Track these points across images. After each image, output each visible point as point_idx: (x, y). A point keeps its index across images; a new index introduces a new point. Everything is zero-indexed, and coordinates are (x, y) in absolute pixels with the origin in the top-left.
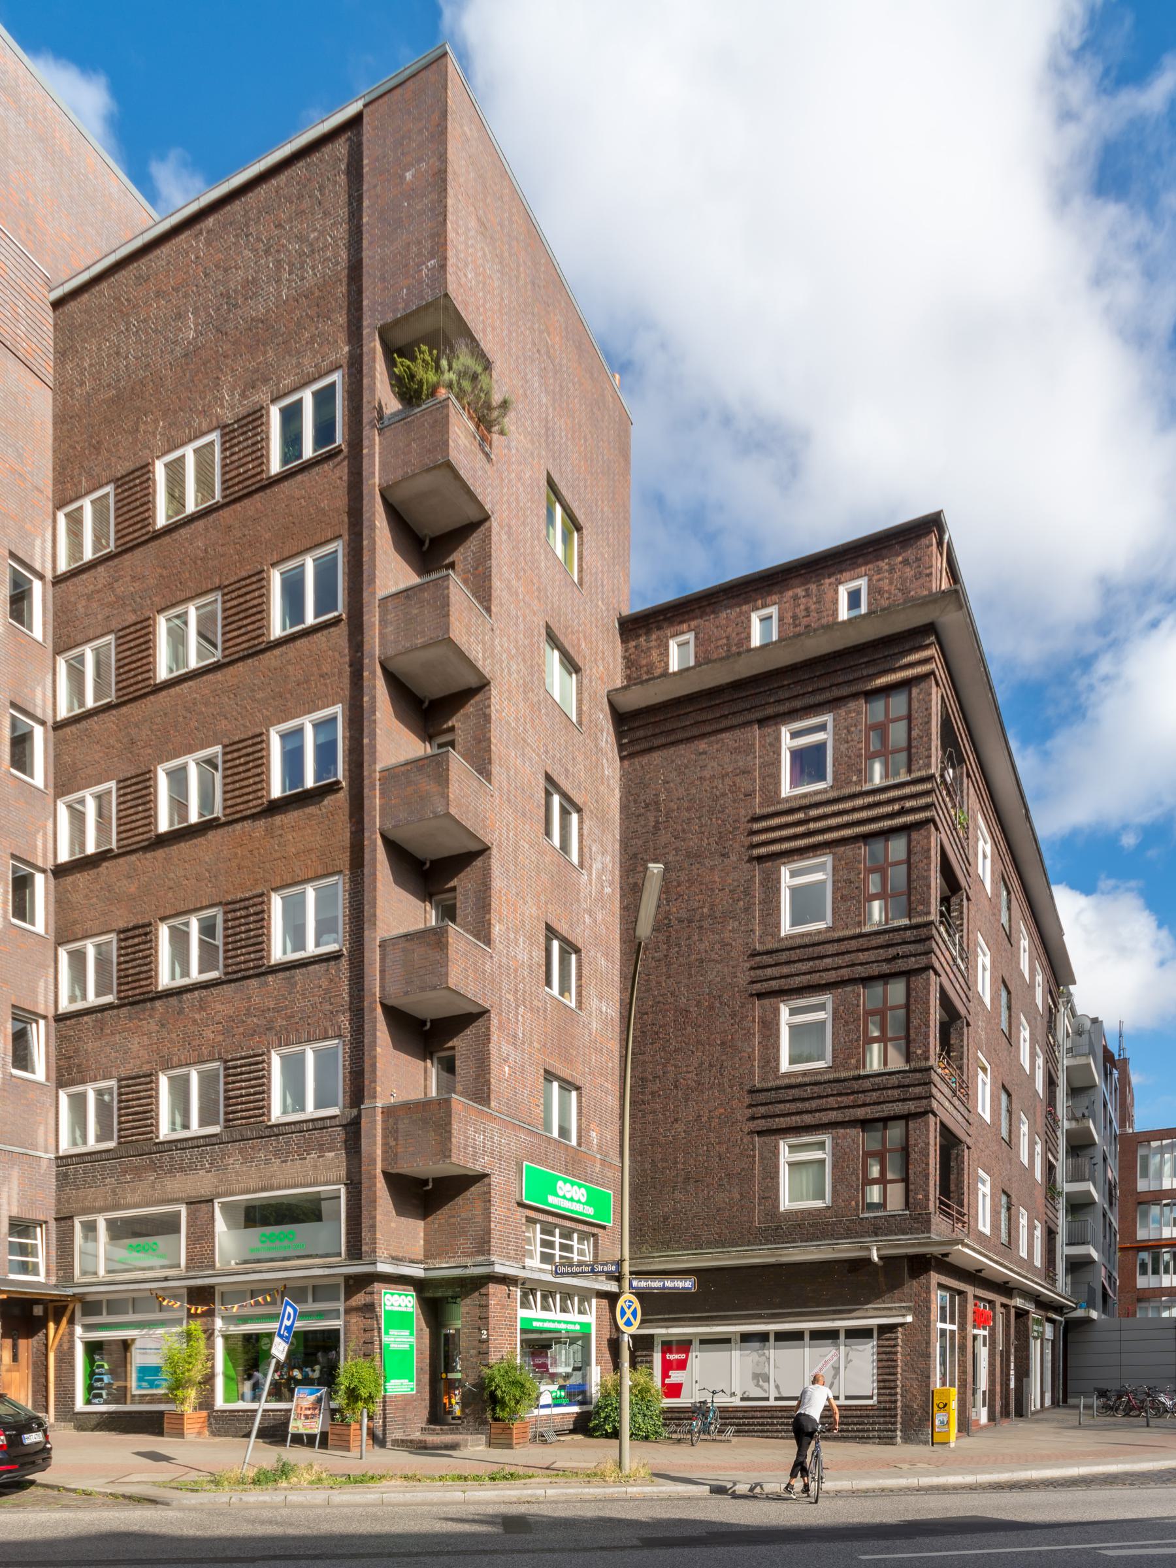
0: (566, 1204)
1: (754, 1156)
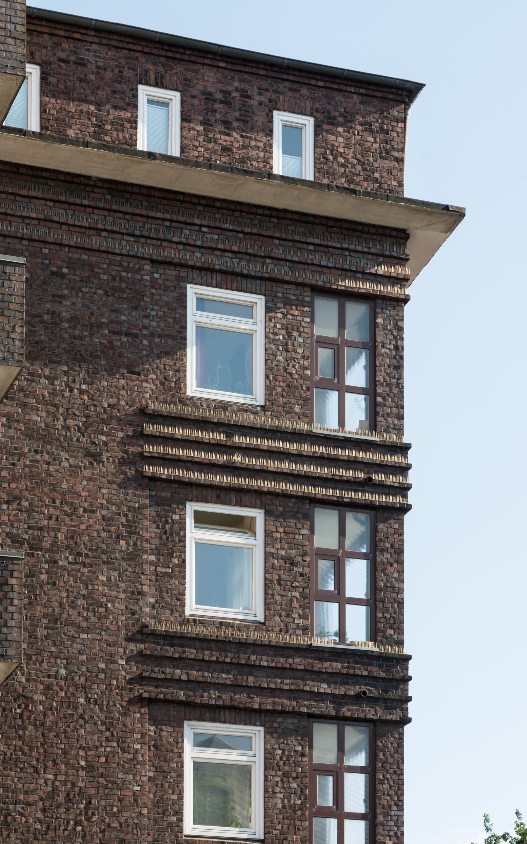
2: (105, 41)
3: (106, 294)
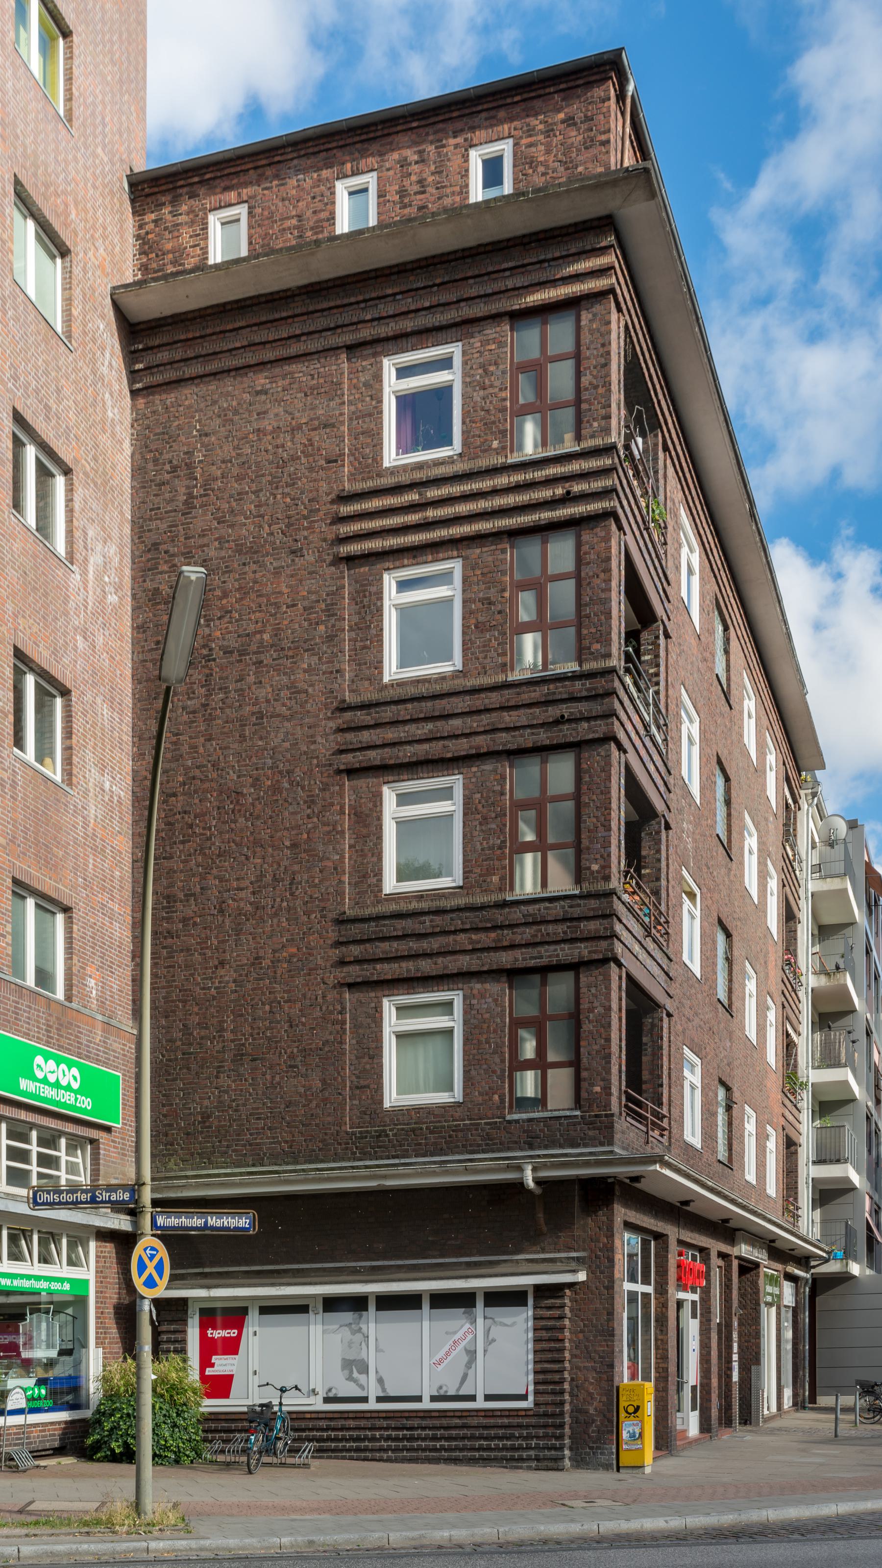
0: (48, 1092)
1: (344, 1022)
2: (302, 152)
3: (306, 395)
